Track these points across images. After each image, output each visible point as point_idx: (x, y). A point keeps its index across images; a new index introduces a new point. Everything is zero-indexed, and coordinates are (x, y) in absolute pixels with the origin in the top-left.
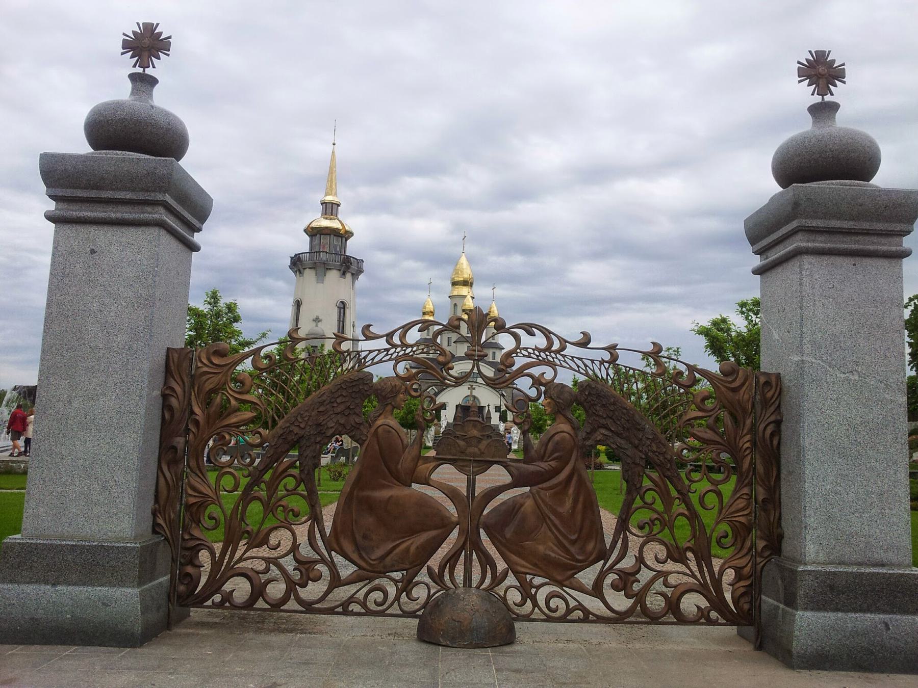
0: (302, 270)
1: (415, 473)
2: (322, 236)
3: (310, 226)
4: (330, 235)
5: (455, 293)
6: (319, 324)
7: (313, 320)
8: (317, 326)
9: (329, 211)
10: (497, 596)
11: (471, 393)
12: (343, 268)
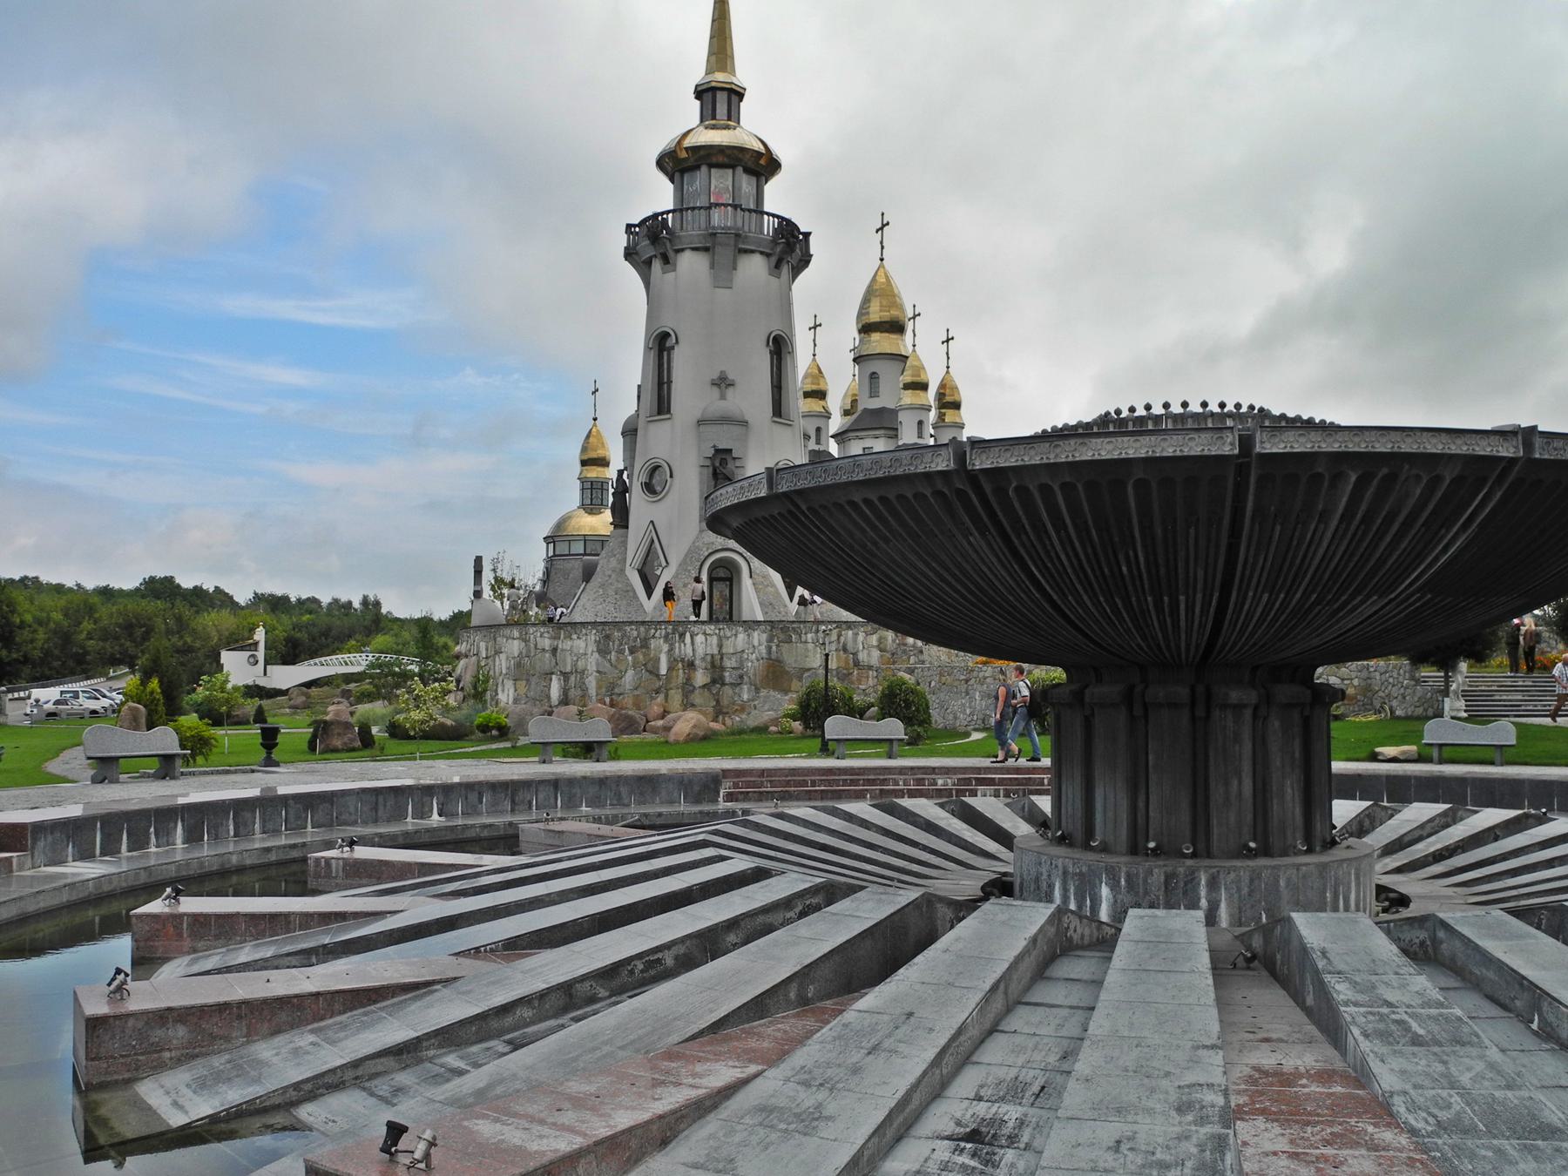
0: (671, 254)
2: (713, 170)
3: (687, 143)
4: (733, 167)
6: (730, 392)
7: (713, 384)
8: (723, 397)
9: (722, 109)
10: (1280, 582)
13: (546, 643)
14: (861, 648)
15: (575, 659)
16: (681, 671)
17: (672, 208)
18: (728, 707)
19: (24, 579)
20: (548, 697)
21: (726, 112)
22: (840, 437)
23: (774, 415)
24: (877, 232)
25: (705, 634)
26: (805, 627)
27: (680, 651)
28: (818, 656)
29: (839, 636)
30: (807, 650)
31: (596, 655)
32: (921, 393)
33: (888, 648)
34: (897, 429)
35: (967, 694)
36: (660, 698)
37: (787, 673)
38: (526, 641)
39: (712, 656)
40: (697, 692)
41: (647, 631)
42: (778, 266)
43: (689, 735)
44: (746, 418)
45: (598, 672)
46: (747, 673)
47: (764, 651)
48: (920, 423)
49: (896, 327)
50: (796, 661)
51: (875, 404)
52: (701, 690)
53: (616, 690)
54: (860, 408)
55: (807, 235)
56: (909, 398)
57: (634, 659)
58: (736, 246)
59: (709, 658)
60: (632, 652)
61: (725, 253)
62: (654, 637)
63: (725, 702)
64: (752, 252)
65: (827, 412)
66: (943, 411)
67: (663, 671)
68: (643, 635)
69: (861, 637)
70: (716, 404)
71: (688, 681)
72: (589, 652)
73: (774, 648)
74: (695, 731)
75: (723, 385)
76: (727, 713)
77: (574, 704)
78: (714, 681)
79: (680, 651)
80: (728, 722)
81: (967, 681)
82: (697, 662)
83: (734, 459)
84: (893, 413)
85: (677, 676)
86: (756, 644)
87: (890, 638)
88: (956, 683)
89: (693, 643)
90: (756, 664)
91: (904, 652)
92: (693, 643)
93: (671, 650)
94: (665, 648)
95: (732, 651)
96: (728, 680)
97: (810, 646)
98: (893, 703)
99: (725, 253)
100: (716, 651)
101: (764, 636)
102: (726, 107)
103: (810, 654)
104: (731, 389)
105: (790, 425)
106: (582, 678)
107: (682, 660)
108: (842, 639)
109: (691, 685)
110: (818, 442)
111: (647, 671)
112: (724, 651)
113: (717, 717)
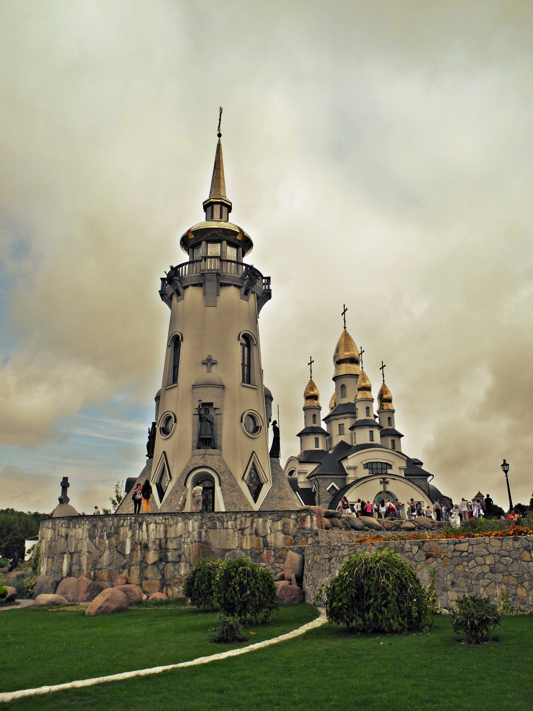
0: (181, 290)
1: (174, 560)
5: (342, 372)
6: (214, 368)
8: (209, 371)
11: (384, 488)
12: (245, 283)
13: (63, 531)
14: (269, 532)
15: (77, 542)
16: (139, 552)
17: (188, 260)
18: (170, 579)
19: (8, 510)
20: (61, 570)
21: (219, 215)
22: (327, 420)
23: (243, 381)
24: (342, 315)
25: (156, 523)
26: (226, 516)
27: (139, 536)
28: (236, 539)
29: (252, 523)
30: (228, 534)
31: (88, 539)
32: (368, 393)
33: (290, 532)
34: (355, 413)
35: (330, 573)
36: (126, 571)
37: (213, 553)
38: (54, 530)
39: (160, 540)
40: (149, 568)
41: (119, 521)
42: (246, 293)
43: (100, 608)
44: (224, 383)
45: (88, 552)
46: (183, 553)
47: (196, 536)
48: (368, 408)
49: (354, 361)
50: (220, 543)
51: (345, 401)
52: (152, 566)
53: (98, 567)
54: (337, 404)
55: (268, 279)
56: (361, 395)
57: (110, 542)
58: (218, 281)
59: (158, 542)
60: (108, 537)
61: (211, 286)
62: (122, 525)
63: (168, 576)
64: (229, 285)
65: (319, 406)
66: (383, 403)
67: (128, 552)
68: (116, 524)
69: (269, 523)
70: (203, 374)
71: (144, 559)
72: (84, 538)
73: (204, 533)
74: (108, 604)
75: (209, 364)
76: (169, 585)
77: (74, 577)
78: (161, 560)
79: (139, 536)
80: (170, 593)
81: (330, 559)
82: (150, 545)
83: (215, 409)
84: (353, 405)
85: (137, 555)
86: (190, 529)
87: (292, 524)
88: (323, 562)
89: (147, 530)
90: (191, 546)
91: (303, 534)
92: (147, 530)
93: (133, 536)
94: (130, 534)
95: (173, 536)
96: (170, 558)
97: (231, 531)
98: (229, 586)
99: (211, 286)
100: (162, 536)
101: (197, 524)
102: (219, 212)
103: (231, 538)
104: (214, 366)
105: (255, 389)
106: (79, 557)
107: (140, 543)
108: (255, 525)
109: (146, 563)
110: (314, 422)
111: (117, 551)
112: (168, 536)
113: (162, 588)
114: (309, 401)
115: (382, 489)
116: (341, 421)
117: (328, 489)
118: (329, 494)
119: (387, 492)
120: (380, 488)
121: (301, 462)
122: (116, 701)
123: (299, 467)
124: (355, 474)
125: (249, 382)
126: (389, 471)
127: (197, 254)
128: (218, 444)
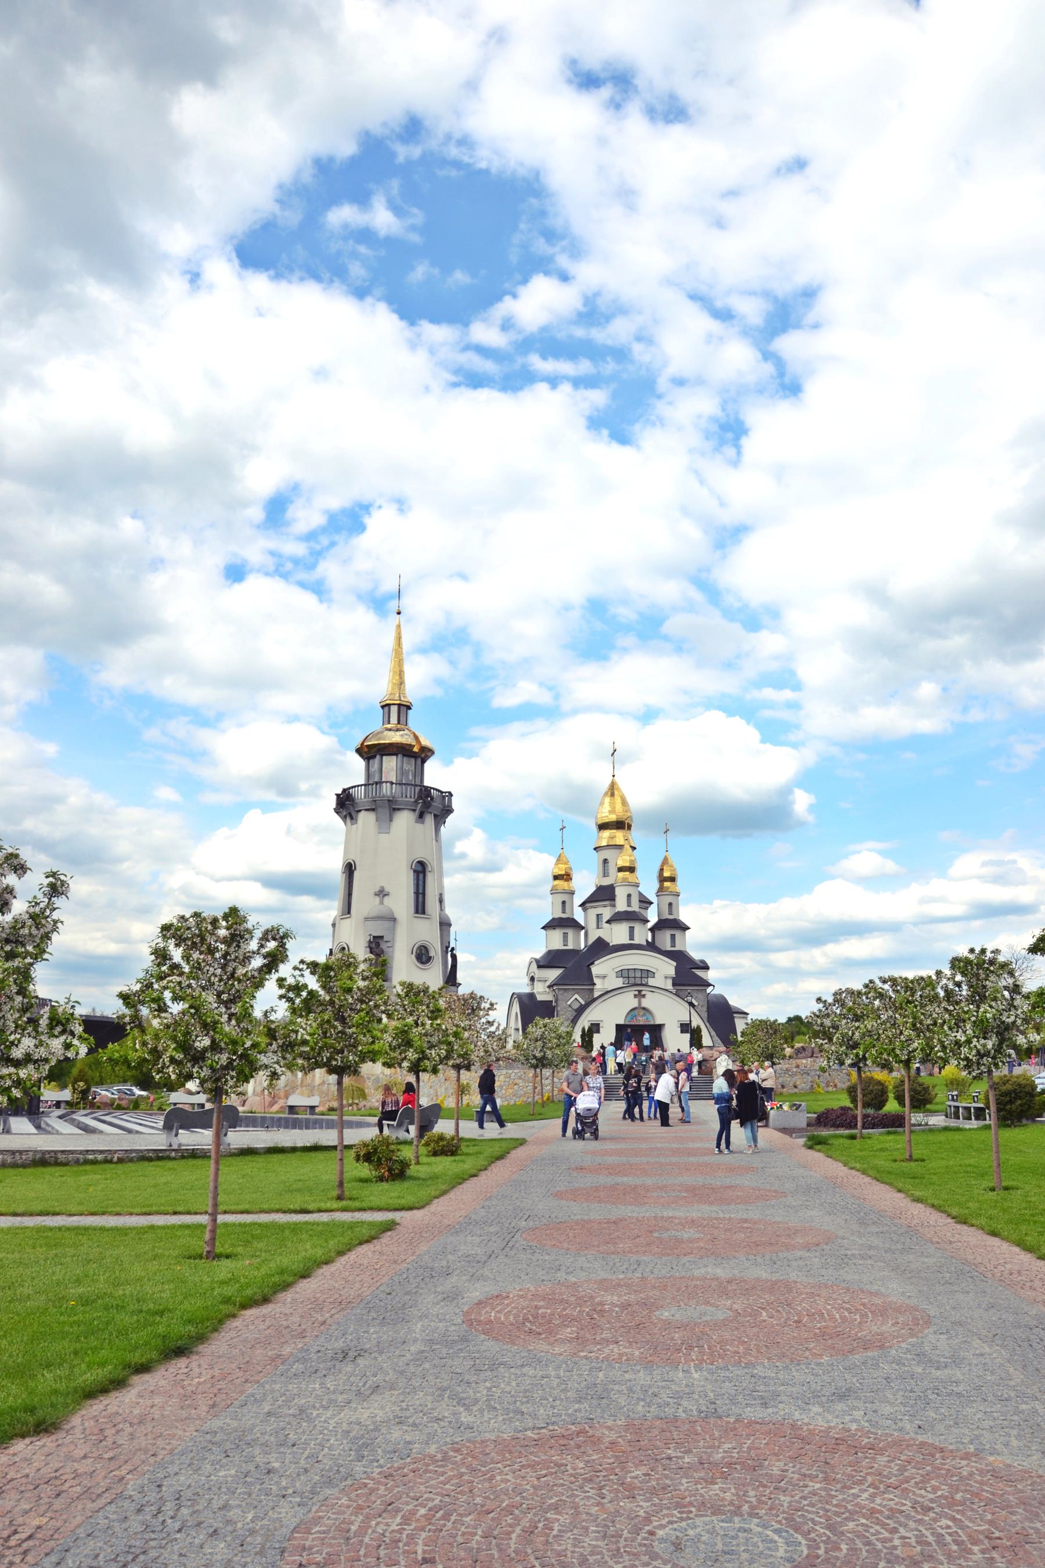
0: (354, 814)
8: (382, 903)
17: (363, 783)
58: (390, 807)
114: (557, 882)
115: (636, 1005)
116: (599, 911)
117: (569, 1003)
118: (570, 1009)
119: (644, 1008)
120: (634, 1003)
121: (539, 967)
122: (368, 1385)
123: (539, 974)
124: (603, 984)
125: (424, 912)
126: (651, 982)
127: (373, 767)
128: (389, 976)
